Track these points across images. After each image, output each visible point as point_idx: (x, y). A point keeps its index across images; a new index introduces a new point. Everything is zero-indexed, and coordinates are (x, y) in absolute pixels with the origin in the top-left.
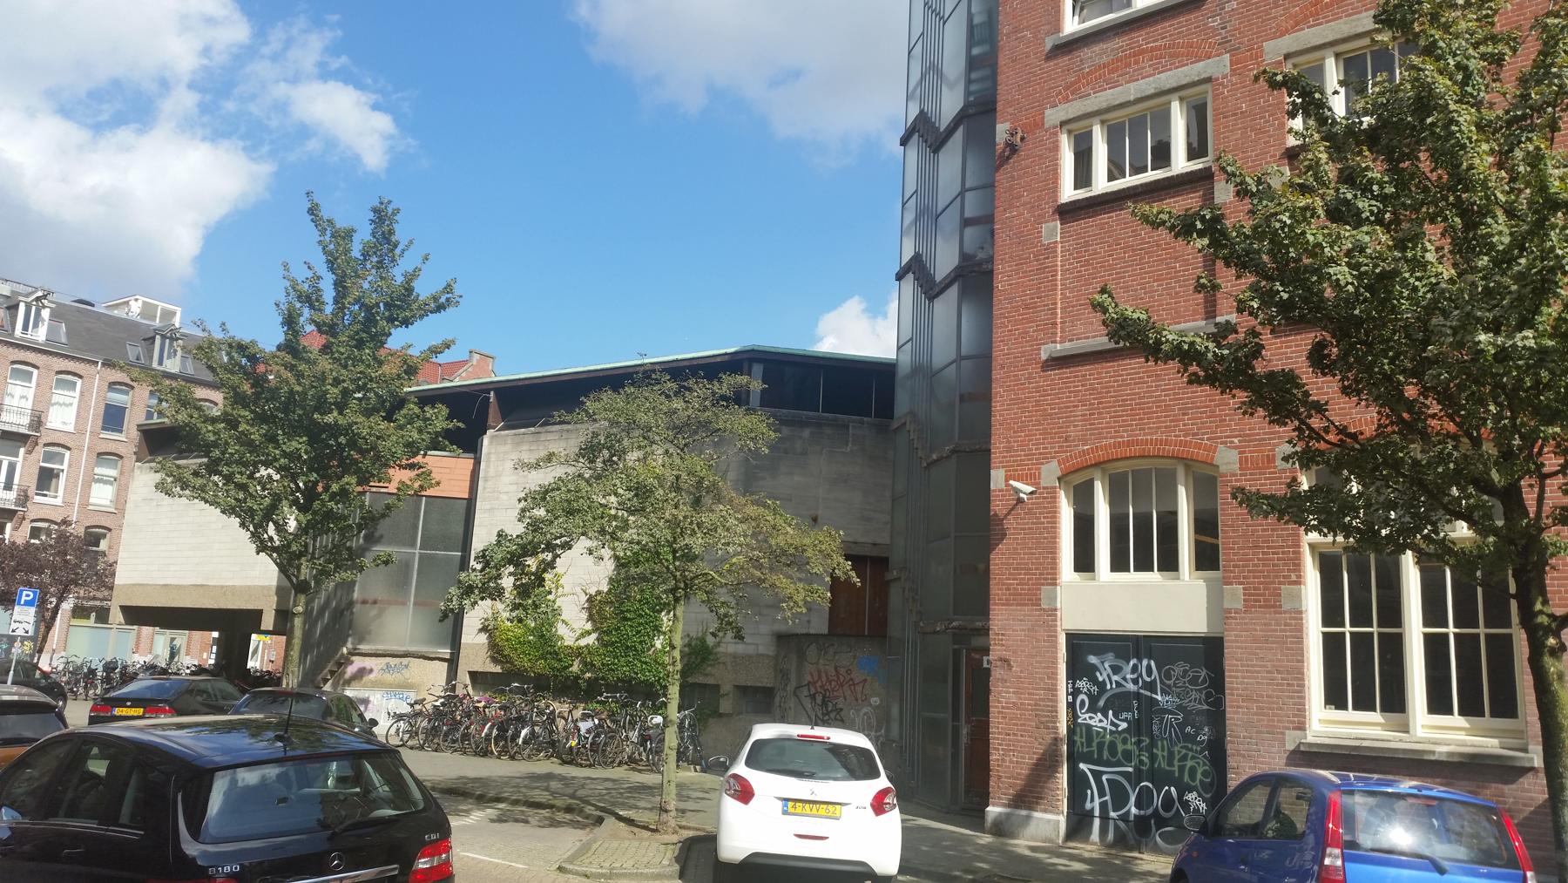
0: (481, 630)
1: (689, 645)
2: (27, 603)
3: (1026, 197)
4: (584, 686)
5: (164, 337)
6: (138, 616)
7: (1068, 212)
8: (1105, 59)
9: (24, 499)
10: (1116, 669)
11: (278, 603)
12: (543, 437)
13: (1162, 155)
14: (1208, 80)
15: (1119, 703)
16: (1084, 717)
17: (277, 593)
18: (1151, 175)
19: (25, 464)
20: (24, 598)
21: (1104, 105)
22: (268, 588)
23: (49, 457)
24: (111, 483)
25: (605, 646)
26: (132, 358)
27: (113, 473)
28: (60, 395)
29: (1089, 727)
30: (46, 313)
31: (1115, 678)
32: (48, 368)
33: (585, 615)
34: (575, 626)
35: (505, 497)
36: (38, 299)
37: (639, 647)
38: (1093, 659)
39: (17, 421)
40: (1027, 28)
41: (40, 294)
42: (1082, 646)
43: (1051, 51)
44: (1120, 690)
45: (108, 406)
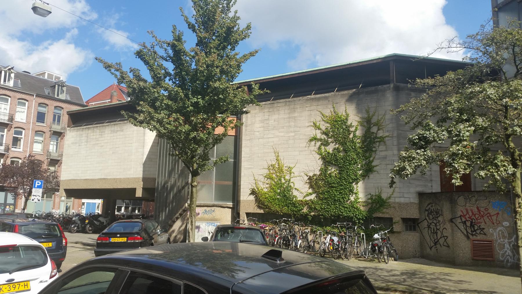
0: (250, 194)
1: (371, 199)
2: (39, 187)
4: (310, 218)
5: (59, 86)
6: (72, 193)
9: (7, 149)
11: (143, 185)
12: (275, 105)
17: (143, 181)
19: (7, 136)
20: (37, 185)
22: (138, 178)
23: (16, 133)
24: (40, 143)
25: (322, 200)
26: (47, 94)
27: (41, 139)
28: (19, 108)
30: (13, 75)
32: (15, 97)
33: (307, 186)
34: (302, 191)
35: (258, 133)
36: (9, 69)
37: (342, 200)
39: (5, 119)
41: (10, 67)
45: (39, 113)
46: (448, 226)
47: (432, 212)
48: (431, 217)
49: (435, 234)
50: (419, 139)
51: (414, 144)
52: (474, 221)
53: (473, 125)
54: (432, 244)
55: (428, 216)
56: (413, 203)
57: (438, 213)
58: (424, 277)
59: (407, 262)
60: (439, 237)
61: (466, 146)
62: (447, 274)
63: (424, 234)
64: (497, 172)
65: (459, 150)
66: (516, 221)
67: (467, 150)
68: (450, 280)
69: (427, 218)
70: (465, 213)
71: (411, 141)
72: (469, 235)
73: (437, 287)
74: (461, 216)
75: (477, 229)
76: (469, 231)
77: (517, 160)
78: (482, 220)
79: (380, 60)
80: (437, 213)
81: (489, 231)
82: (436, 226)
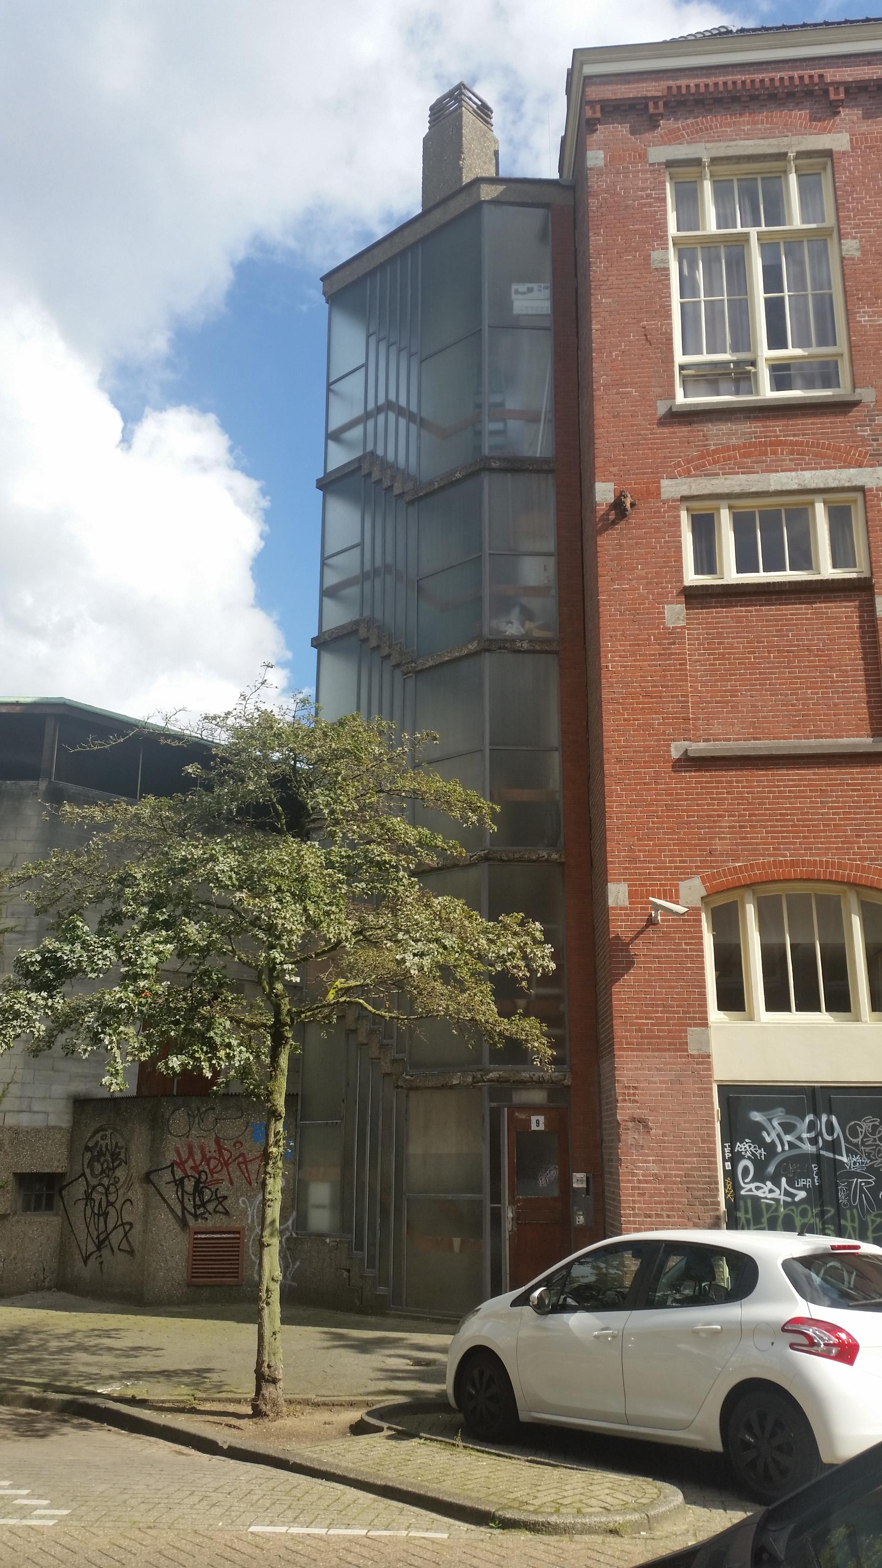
3: (640, 570)
7: (695, 597)
8: (734, 441)
10: (788, 1128)
13: (804, 557)
14: (861, 489)
15: (793, 1167)
16: (748, 1188)
18: (788, 575)
21: (737, 490)
29: (756, 1200)
31: (787, 1138)
38: (756, 1116)
40: (632, 384)
42: (739, 1100)
43: (665, 417)
44: (795, 1152)
46: (137, 1193)
47: (101, 1154)
48: (98, 1167)
49: (102, 1219)
50: (44, 963)
51: (27, 974)
52: (203, 1177)
53: (177, 937)
54: (92, 1248)
55: (90, 1165)
56: (54, 1127)
57: (117, 1157)
58: (43, 1347)
59: (13, 1305)
60: (110, 1226)
61: (143, 992)
62: (107, 1333)
63: (72, 1219)
64: (210, 1060)
65: (122, 1002)
66: (265, 1179)
67: (143, 1001)
68: (110, 1349)
69: (87, 1171)
70: (184, 1156)
71: (22, 966)
72: (188, 1216)
73: (65, 1373)
74: (172, 1165)
75: (209, 1201)
76: (190, 1207)
77: (286, 1024)
78: (224, 1175)
79: (18, 709)
80: (115, 1156)
81: (237, 1202)
82: (107, 1193)
